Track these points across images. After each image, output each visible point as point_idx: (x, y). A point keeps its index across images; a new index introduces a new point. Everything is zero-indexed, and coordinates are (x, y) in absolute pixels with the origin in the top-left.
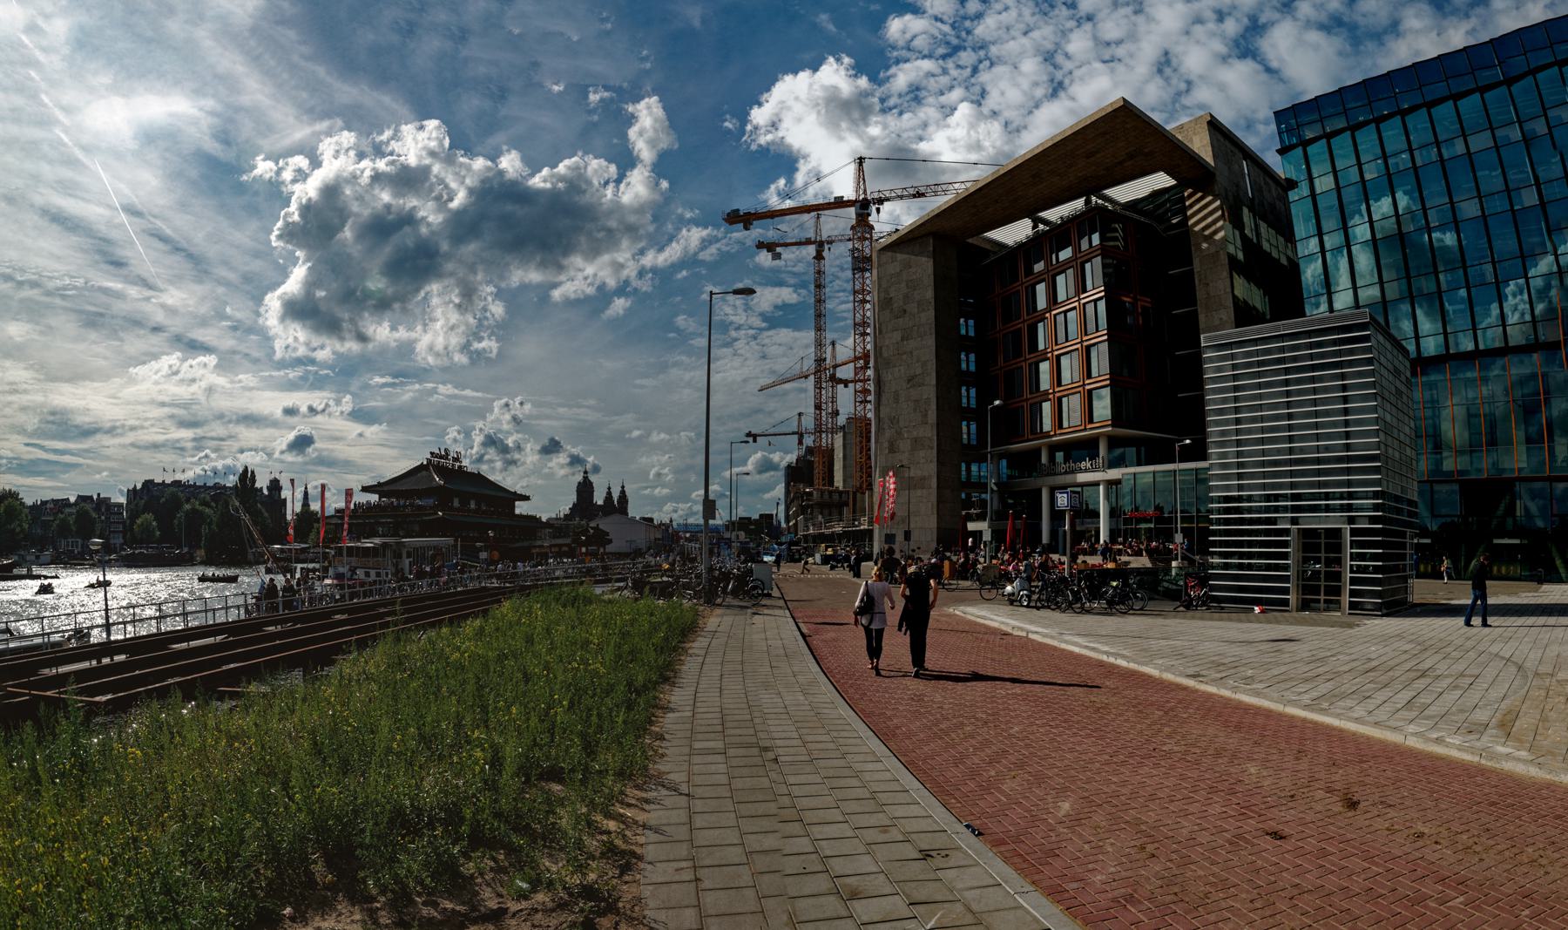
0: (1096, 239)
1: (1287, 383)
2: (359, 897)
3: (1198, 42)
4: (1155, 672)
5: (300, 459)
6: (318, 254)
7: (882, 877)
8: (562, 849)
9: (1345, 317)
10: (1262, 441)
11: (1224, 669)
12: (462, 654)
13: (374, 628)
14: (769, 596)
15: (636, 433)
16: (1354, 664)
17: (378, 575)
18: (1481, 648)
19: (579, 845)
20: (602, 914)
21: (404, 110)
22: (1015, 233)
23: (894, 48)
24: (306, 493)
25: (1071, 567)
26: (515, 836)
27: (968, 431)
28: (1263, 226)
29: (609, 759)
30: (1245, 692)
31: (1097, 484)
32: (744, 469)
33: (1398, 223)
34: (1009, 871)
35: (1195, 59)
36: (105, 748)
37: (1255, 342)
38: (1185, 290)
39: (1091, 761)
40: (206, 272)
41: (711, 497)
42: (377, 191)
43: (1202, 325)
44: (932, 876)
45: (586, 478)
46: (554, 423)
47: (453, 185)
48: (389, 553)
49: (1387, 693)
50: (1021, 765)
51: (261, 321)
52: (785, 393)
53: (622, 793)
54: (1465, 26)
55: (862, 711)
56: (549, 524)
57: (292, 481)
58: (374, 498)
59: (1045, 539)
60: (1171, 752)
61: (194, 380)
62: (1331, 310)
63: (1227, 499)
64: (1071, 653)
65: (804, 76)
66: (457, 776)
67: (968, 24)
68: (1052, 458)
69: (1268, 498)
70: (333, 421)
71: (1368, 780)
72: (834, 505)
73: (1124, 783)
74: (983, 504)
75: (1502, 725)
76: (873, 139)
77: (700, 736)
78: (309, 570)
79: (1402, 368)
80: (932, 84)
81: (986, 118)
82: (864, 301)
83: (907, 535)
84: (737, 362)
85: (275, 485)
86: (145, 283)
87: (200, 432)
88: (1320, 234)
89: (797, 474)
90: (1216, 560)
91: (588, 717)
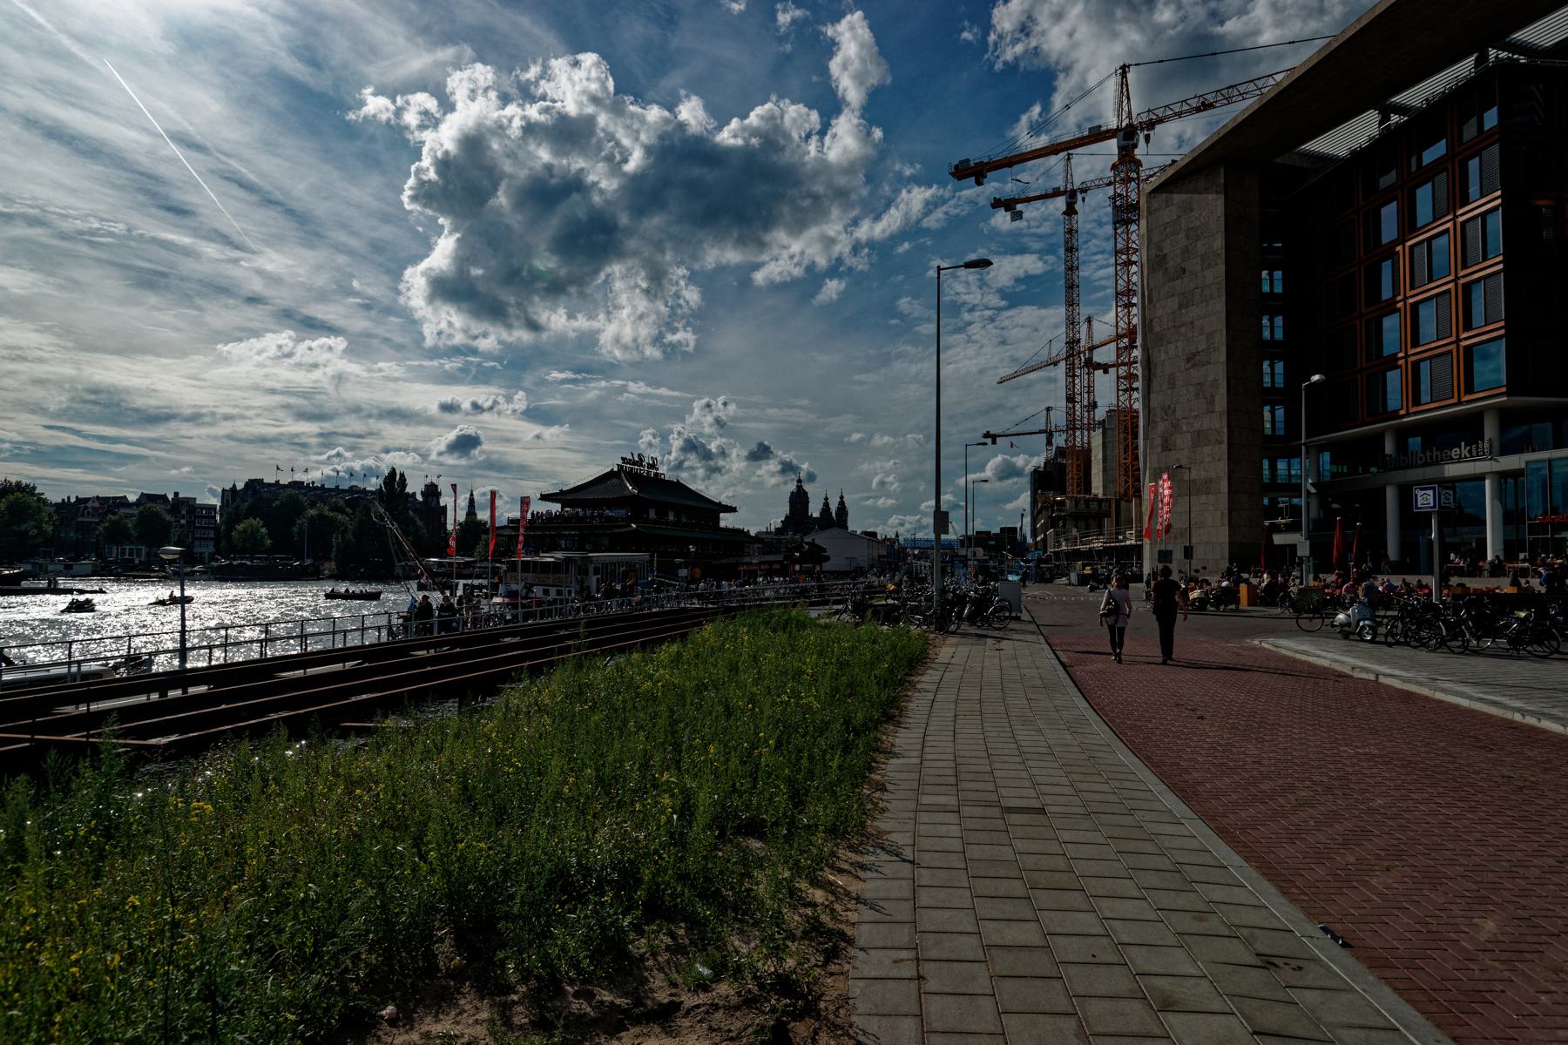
2: (492, 987)
5: (463, 462)
6: (467, 223)
8: (756, 924)
12: (655, 683)
13: (551, 652)
14: (1018, 619)
15: (856, 437)
17: (559, 593)
19: (778, 919)
20: (798, 1016)
21: (549, 38)
24: (472, 501)
26: (694, 904)
27: (1272, 418)
29: (819, 811)
31: (1481, 478)
32: (982, 476)
36: (153, 807)
40: (317, 234)
41: (944, 508)
42: (532, 147)
45: (799, 488)
46: (763, 426)
47: (626, 142)
48: (573, 569)
51: (402, 300)
52: (1030, 385)
53: (833, 854)
56: (758, 538)
57: (454, 487)
58: (555, 508)
59: (1392, 552)
61: (315, 366)
64: (1456, 707)
66: (638, 827)
68: (1401, 446)
70: (503, 420)
72: (1091, 516)
74: (1295, 511)
76: (1159, 30)
77: (929, 789)
78: (473, 587)
82: (1130, 263)
83: (1188, 552)
85: (432, 491)
86: (225, 240)
87: (327, 426)
89: (1044, 481)
91: (799, 759)
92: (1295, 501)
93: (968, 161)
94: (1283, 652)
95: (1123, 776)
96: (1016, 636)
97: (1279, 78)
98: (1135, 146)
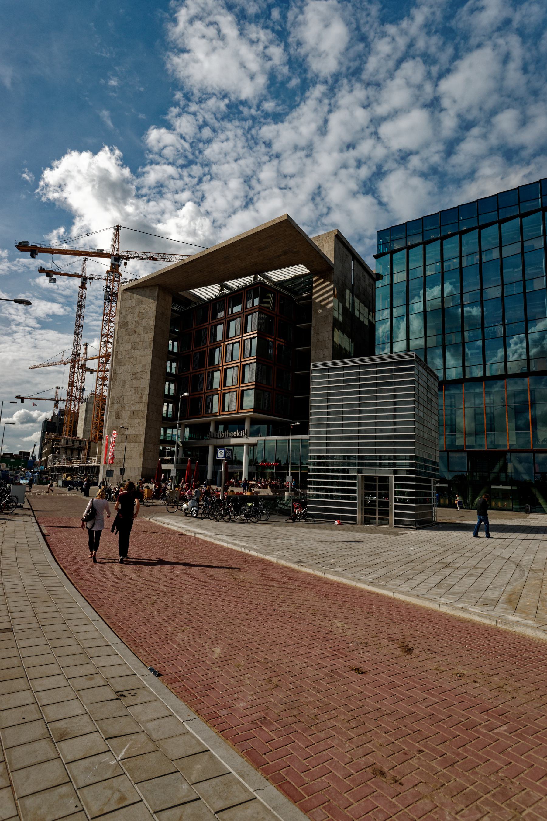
0: (257, 302)
1: (360, 393)
3: (341, 181)
4: (274, 560)
7: (86, 717)
9: (400, 356)
10: (342, 425)
11: (317, 558)
16: (400, 558)
18: (487, 551)
22: (209, 292)
23: (151, 152)
25: (224, 494)
27: (167, 409)
28: (357, 301)
30: (330, 573)
31: (242, 445)
32: (10, 420)
33: (443, 302)
34: (180, 704)
35: (336, 193)
37: (343, 368)
38: (305, 337)
39: (234, 618)
43: (312, 358)
44: (124, 712)
49: (423, 577)
50: (188, 622)
52: (48, 373)
54: (525, 171)
55: (82, 587)
59: (209, 476)
60: (285, 612)
62: (391, 352)
63: (319, 457)
65: (86, 155)
67: (201, 145)
68: (216, 429)
69: (344, 458)
71: (417, 633)
73: (255, 634)
75: (509, 601)
76: (128, 215)
79: (433, 386)
80: (172, 184)
81: (202, 215)
83: (122, 471)
84: (15, 347)
88: (391, 308)
89: (49, 427)
90: (312, 493)
92: (173, 449)
93: (27, 242)
94: (159, 523)
95: (64, 600)
96: (17, 518)
97: (185, 257)
98: (119, 266)
